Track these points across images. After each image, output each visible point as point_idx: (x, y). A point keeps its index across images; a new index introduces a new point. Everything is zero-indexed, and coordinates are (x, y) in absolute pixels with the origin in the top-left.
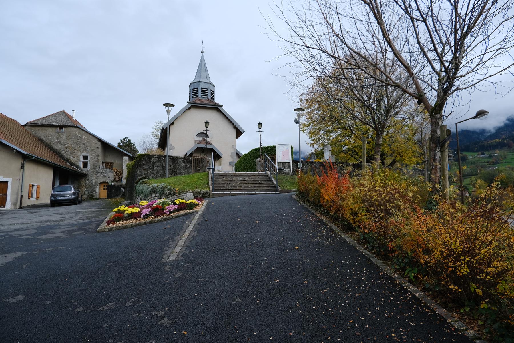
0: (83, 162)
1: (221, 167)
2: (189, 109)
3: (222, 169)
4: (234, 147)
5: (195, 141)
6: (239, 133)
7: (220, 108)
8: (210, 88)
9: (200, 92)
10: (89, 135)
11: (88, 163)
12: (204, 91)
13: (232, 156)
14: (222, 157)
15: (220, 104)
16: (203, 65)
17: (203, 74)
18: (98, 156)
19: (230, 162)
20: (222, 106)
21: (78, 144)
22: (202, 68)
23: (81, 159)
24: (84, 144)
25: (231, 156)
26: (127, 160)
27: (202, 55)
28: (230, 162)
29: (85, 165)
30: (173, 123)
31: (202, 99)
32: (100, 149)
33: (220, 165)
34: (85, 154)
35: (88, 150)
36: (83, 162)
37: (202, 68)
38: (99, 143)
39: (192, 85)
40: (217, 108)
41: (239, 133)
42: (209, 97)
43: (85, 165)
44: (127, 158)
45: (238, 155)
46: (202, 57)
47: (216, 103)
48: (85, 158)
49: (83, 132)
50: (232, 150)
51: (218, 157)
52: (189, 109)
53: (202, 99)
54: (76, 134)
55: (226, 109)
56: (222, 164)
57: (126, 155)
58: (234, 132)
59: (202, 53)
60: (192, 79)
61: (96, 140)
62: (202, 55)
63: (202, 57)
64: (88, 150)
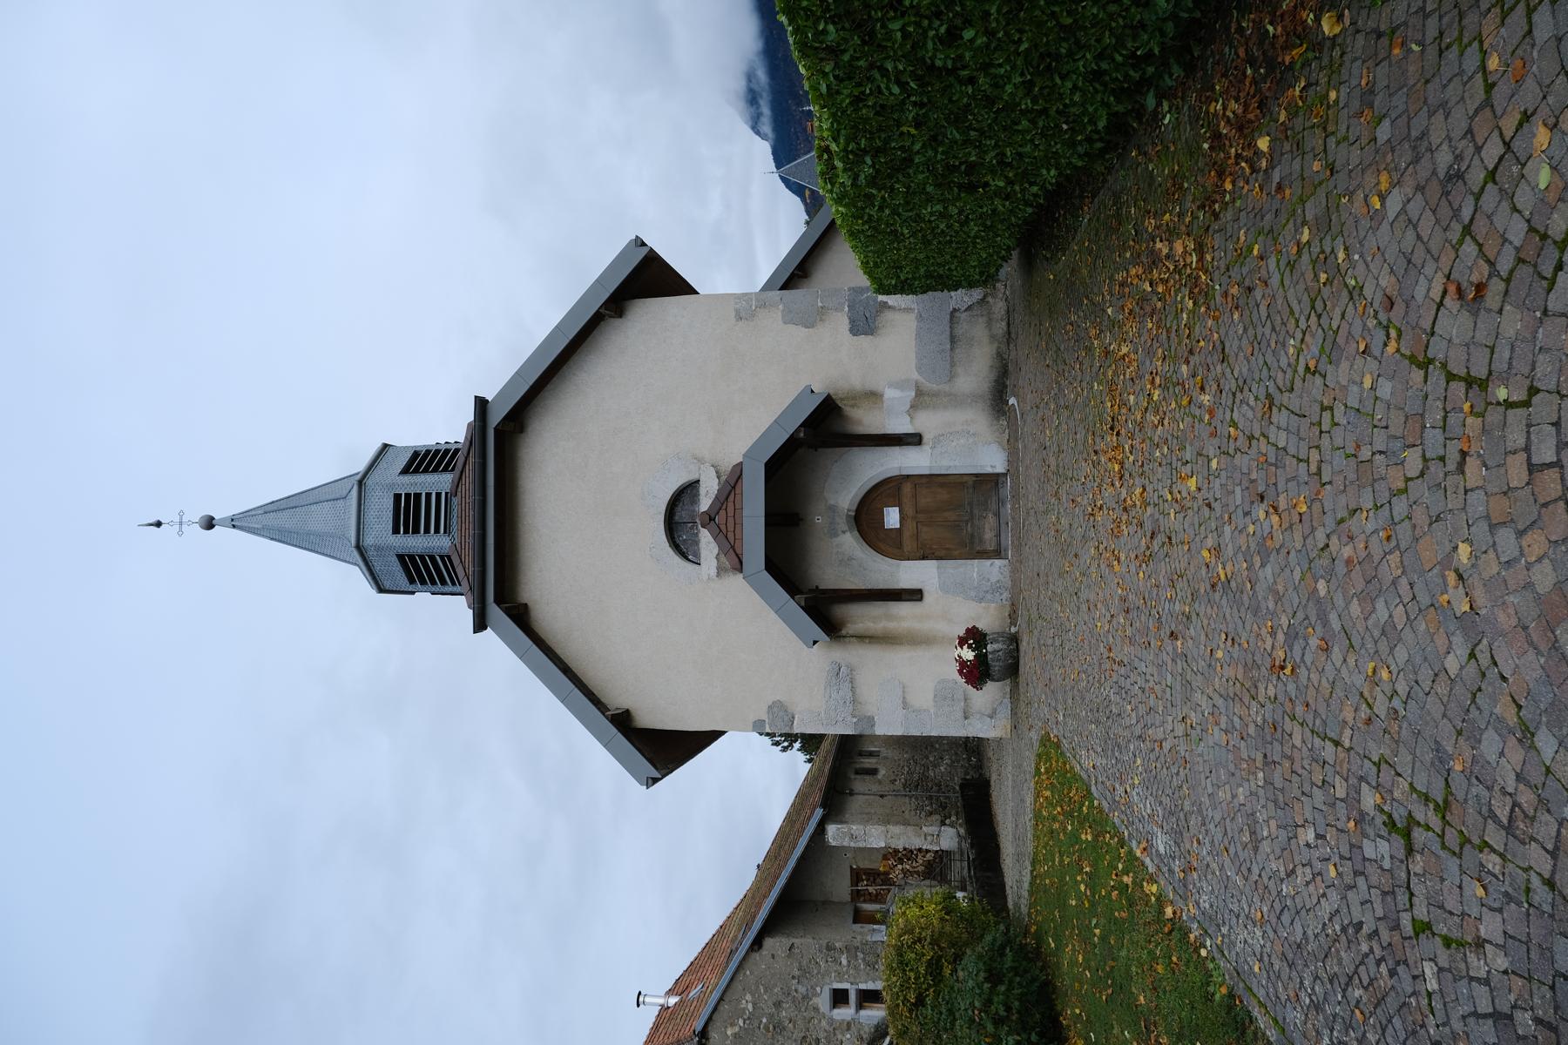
0: (860, 1007)
1: (890, 394)
2: (521, 617)
3: (900, 385)
4: (745, 309)
5: (721, 571)
6: (648, 278)
7: (495, 417)
8: (392, 479)
9: (417, 543)
10: (738, 986)
11: (863, 986)
12: (408, 514)
13: (810, 319)
14: (820, 388)
15: (469, 415)
16: (271, 520)
17: (319, 518)
18: (829, 948)
19: (855, 331)
20: (481, 404)
21: (779, 1028)
22: (283, 521)
23: (845, 1013)
24: (778, 1004)
25: (809, 325)
26: (844, 828)
27: (223, 523)
28: (855, 331)
29: (868, 998)
30: (623, 722)
31: (456, 522)
32: (797, 941)
33: (874, 396)
34: (823, 1001)
35: (802, 989)
36: (860, 1007)
37: (283, 521)
38: (769, 942)
39: (387, 585)
40: (503, 432)
41: (648, 278)
42: (441, 482)
43: (868, 998)
44: (832, 830)
45: (798, 273)
46: (234, 523)
47: (470, 441)
48: (839, 998)
49: (725, 1007)
50: (772, 320)
51: (824, 428)
52: (521, 617)
53: (456, 522)
54: (735, 1035)
55: (495, 370)
56: (872, 385)
57: (821, 829)
58: (651, 313)
59: (209, 524)
60: (355, 576)
61: (756, 956)
62: (223, 523)
63: (234, 523)
64: (802, 989)
